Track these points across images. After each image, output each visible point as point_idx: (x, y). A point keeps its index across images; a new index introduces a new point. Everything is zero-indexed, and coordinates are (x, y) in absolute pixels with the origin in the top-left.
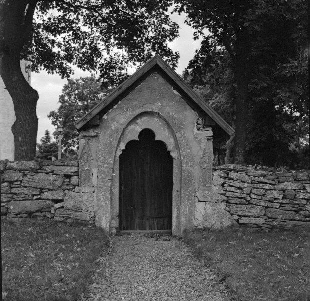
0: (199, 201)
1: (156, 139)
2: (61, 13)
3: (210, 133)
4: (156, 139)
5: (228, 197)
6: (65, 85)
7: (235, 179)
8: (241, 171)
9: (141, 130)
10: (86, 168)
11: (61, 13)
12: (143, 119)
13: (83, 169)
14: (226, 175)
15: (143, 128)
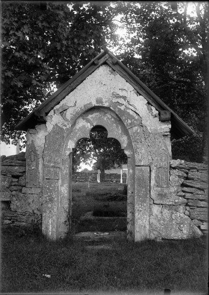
0: (154, 204)
1: (109, 136)
2: (184, 51)
3: (167, 127)
4: (109, 136)
5: (188, 199)
6: (2, 84)
7: (196, 179)
8: (202, 170)
9: (92, 127)
10: (33, 168)
11: (184, 51)
12: (94, 115)
13: (30, 169)
14: (185, 175)
15: (95, 124)
